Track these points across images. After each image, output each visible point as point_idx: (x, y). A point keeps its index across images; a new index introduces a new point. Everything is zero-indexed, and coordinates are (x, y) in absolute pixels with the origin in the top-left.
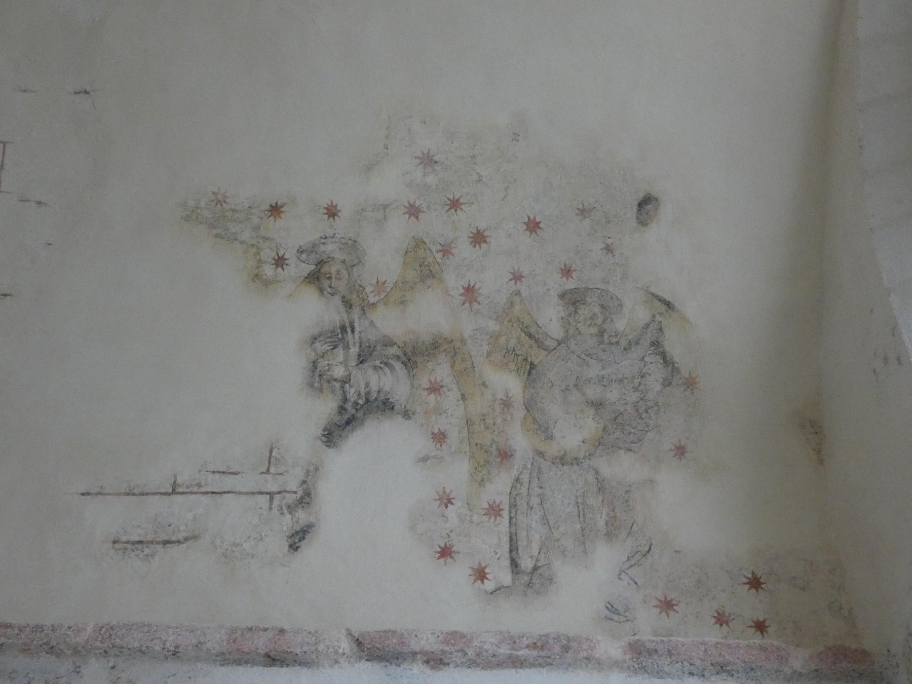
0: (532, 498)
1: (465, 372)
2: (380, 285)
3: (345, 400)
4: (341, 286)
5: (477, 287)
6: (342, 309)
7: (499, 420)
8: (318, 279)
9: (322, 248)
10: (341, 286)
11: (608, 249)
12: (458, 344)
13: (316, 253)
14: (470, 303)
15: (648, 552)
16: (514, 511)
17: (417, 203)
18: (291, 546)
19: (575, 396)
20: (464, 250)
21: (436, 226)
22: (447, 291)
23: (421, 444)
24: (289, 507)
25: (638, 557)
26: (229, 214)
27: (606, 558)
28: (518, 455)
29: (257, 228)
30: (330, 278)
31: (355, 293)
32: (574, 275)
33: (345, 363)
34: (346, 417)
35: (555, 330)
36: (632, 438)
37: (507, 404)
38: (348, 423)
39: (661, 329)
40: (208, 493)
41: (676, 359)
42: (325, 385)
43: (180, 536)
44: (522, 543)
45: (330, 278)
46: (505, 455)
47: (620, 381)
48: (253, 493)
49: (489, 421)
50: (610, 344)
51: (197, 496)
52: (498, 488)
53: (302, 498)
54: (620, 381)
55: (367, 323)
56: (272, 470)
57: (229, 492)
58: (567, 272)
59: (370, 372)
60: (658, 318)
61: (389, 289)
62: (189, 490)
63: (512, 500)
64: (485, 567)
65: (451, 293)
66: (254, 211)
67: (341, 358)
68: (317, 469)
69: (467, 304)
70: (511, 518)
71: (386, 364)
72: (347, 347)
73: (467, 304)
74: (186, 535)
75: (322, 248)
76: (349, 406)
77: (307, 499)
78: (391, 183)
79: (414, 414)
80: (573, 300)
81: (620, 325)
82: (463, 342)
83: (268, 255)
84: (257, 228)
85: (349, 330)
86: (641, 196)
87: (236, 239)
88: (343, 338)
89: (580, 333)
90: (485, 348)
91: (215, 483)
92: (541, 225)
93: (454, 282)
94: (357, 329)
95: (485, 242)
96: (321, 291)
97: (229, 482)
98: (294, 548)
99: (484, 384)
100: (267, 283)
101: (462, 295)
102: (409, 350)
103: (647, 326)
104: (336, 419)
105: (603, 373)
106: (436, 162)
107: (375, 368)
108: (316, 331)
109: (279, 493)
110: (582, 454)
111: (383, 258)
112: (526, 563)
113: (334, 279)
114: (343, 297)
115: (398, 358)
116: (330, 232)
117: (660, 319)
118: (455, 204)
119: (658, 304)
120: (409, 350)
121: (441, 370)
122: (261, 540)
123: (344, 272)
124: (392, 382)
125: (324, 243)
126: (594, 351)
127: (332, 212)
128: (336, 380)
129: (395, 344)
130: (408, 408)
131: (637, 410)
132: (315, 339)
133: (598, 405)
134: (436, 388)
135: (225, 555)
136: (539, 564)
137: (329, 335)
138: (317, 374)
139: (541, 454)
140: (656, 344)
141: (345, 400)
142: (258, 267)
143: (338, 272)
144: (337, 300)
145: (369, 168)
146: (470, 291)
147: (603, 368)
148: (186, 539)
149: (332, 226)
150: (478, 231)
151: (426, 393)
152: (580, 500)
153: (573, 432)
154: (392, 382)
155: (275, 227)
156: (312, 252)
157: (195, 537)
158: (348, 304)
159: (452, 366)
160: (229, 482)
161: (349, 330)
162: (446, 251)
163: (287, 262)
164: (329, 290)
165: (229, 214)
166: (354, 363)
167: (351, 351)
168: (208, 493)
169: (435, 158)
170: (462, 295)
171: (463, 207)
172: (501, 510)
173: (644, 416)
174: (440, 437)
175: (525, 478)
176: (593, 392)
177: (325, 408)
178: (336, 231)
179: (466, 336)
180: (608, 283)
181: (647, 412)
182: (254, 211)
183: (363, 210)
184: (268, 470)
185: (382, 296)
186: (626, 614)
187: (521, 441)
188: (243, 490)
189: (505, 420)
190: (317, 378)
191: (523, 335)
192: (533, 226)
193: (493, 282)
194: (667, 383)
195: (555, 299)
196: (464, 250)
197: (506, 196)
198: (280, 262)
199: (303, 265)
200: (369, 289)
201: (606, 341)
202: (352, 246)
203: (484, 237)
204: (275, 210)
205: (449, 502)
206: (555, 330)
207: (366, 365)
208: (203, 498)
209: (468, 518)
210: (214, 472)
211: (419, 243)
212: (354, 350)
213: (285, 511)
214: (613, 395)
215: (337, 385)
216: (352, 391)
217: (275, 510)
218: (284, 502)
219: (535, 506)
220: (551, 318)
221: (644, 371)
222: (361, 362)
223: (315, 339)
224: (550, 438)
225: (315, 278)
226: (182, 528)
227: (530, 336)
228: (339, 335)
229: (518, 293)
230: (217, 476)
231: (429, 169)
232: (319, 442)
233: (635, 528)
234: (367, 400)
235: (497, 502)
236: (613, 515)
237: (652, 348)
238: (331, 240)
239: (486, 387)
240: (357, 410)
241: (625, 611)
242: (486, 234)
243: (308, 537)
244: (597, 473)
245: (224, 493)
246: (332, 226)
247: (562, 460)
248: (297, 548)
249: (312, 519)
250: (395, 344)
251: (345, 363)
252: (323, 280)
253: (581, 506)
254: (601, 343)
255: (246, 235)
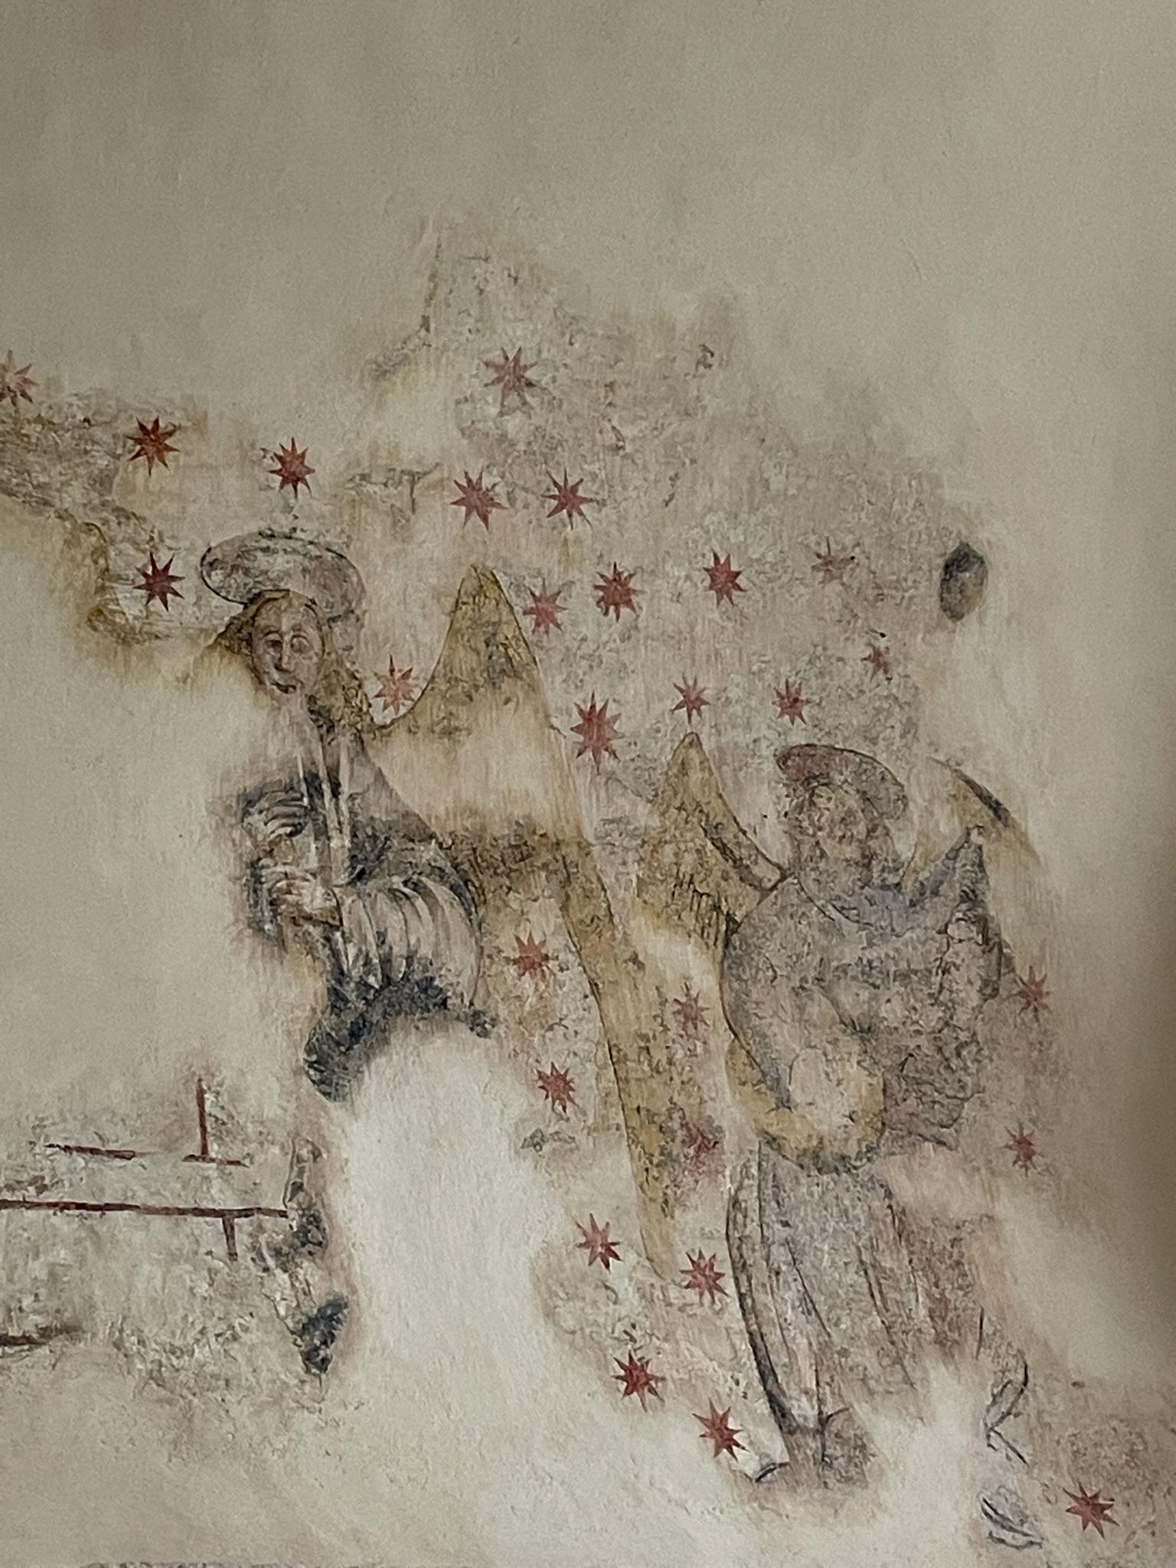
0: (774, 1248)
1: (592, 928)
2: (396, 679)
3: (340, 975)
4: (305, 667)
5: (608, 715)
6: (310, 732)
7: (680, 1055)
8: (249, 643)
9: (262, 561)
10: (305, 667)
11: (878, 660)
12: (572, 853)
13: (247, 572)
14: (596, 753)
15: (1025, 1383)
16: (743, 1278)
17: (486, 482)
18: (308, 1357)
19: (818, 1007)
20: (581, 611)
21: (522, 546)
22: (547, 716)
23: (522, 1102)
24: (277, 1253)
25: (1010, 1395)
26: (34, 430)
27: (953, 1395)
28: (729, 1142)
29: (103, 481)
30: (277, 644)
31: (340, 692)
32: (806, 711)
33: (322, 872)
34: (349, 1018)
35: (774, 842)
36: (940, 1114)
37: (690, 1014)
38: (355, 1035)
39: (981, 865)
40: (66, 1206)
41: (1006, 937)
42: (289, 931)
43: (31, 1324)
44: (779, 1358)
45: (277, 644)
46: (704, 1141)
47: (904, 977)
48: (182, 1212)
49: (659, 1055)
50: (884, 887)
51: (43, 1212)
52: (699, 1224)
53: (304, 1230)
54: (904, 977)
55: (368, 777)
56: (214, 1150)
57: (122, 1207)
58: (791, 703)
59: (383, 903)
60: (974, 836)
61: (416, 694)
62: (18, 1196)
63: (735, 1252)
64: (725, 1415)
65: (555, 722)
66: (98, 433)
67: (313, 864)
68: (316, 1155)
69: (589, 754)
70: (741, 1297)
71: (416, 887)
72: (322, 833)
73: (589, 754)
74: (41, 1321)
75: (262, 561)
76: (350, 991)
77: (315, 1234)
78: (425, 421)
79: (494, 1022)
80: (805, 770)
81: (904, 846)
82: (585, 848)
83: (128, 559)
84: (103, 481)
85: (326, 788)
86: (952, 546)
87: (46, 503)
88: (313, 808)
89: (823, 854)
90: (635, 871)
91: (76, 1178)
92: (741, 581)
93: (563, 698)
94: (345, 789)
95: (629, 603)
96: (257, 675)
97: (113, 1180)
98: (316, 1362)
99: (635, 959)
100: (126, 637)
101: (577, 729)
102: (464, 854)
103: (954, 854)
104: (329, 1022)
105: (869, 954)
106: (530, 384)
107: (394, 894)
108: (250, 783)
109: (246, 1213)
110: (852, 1149)
111: (403, 612)
112: (803, 1409)
113: (286, 647)
114: (312, 699)
115: (440, 874)
116: (283, 523)
117: (980, 840)
118: (568, 499)
119: (977, 804)
120: (464, 854)
121: (539, 918)
122: (235, 1338)
123: (311, 632)
124: (426, 933)
125: (266, 550)
126: (852, 901)
127: (292, 471)
128: (309, 918)
129: (432, 836)
130: (478, 1006)
131: (940, 1049)
132: (248, 802)
133: (864, 1030)
134: (532, 961)
135: (155, 1377)
136: (828, 1410)
137: (282, 796)
138: (264, 895)
139: (772, 1141)
140: (971, 897)
141: (340, 975)
142: (102, 589)
143: (297, 629)
144: (296, 704)
145: (381, 373)
146: (593, 723)
147: (871, 945)
148: (46, 1333)
149: (288, 509)
150: (617, 574)
151: (512, 970)
152: (866, 1257)
153: (832, 1096)
154: (426, 933)
155: (144, 481)
156: (235, 568)
157: (70, 1331)
158: (323, 720)
159: (564, 908)
160: (113, 1180)
161: (326, 788)
162: (544, 612)
163: (175, 585)
164: (276, 676)
165: (34, 430)
166: (343, 878)
167: (334, 843)
168: (66, 1206)
169: (528, 374)
170: (577, 729)
171: (583, 508)
172: (720, 1275)
173: (954, 1063)
174: (557, 1086)
175: (749, 1199)
176: (853, 998)
177: (300, 990)
178: (299, 523)
179: (589, 834)
180: (874, 741)
181: (959, 1055)
182: (98, 433)
183: (363, 477)
184: (204, 1149)
185: (403, 711)
186: (1025, 1529)
187: (729, 1108)
188: (152, 1202)
189: (692, 1053)
190: (270, 914)
191: (710, 846)
192: (724, 580)
193: (641, 709)
194: (990, 990)
195: (770, 767)
196: (581, 611)
197: (672, 497)
198: (158, 583)
199: (216, 601)
200: (372, 687)
201: (877, 881)
202: (334, 567)
203: (629, 592)
204: (152, 440)
205: (609, 1252)
206: (774, 842)
207: (371, 886)
208: (58, 1219)
209: (658, 1293)
210: (67, 1148)
211: (484, 583)
212: (340, 843)
213: (271, 1263)
214: (892, 1011)
215: (316, 932)
216: (352, 951)
217: (245, 1258)
218: (263, 1239)
219: (784, 1268)
220: (763, 808)
221: (947, 958)
222: (360, 876)
223: (250, 803)
224: (785, 1103)
225: (242, 638)
226: (27, 1302)
227: (723, 849)
228: (303, 799)
229: (695, 742)
230: (80, 1161)
231: (513, 399)
232: (306, 1082)
233: (988, 1329)
234: (387, 980)
235: (707, 1256)
236: (940, 1305)
237: (964, 907)
238: (282, 544)
239: (641, 966)
240: (368, 1003)
241: (1022, 1522)
242: (632, 584)
243: (340, 1332)
244: (889, 1194)
245: (108, 1207)
246: (288, 509)
247: (817, 1159)
248: (325, 1361)
249: (340, 1288)
250: (432, 836)
251: (322, 872)
252: (261, 647)
253: (870, 1272)
254: (867, 883)
255: (74, 496)
